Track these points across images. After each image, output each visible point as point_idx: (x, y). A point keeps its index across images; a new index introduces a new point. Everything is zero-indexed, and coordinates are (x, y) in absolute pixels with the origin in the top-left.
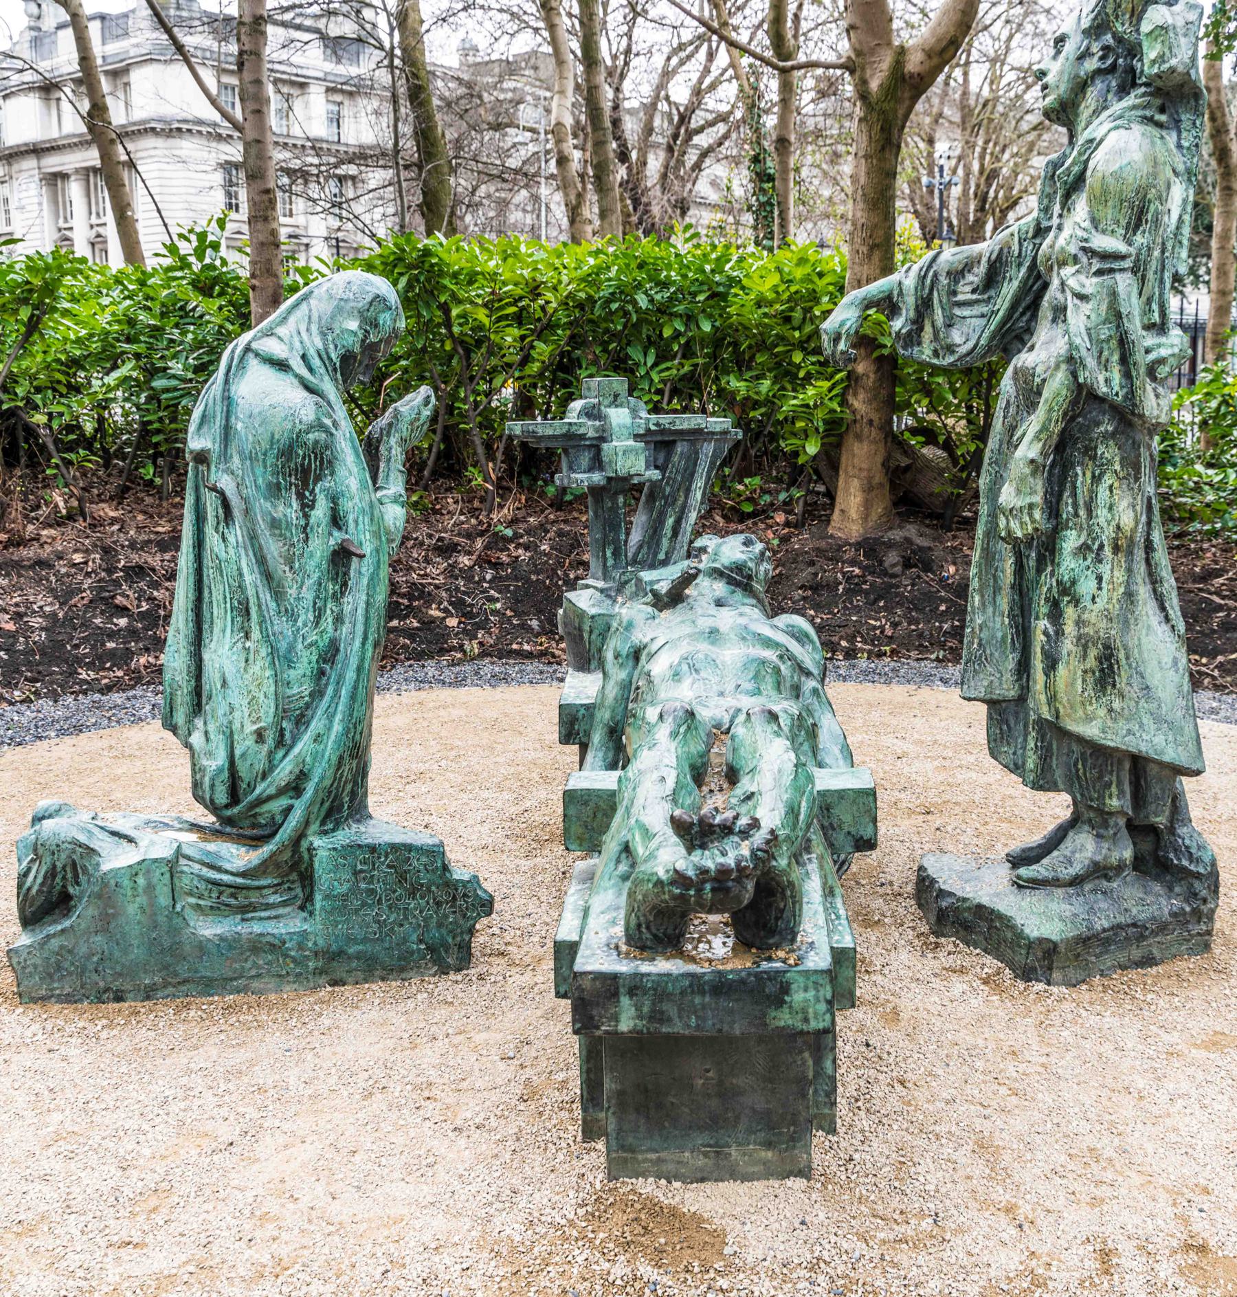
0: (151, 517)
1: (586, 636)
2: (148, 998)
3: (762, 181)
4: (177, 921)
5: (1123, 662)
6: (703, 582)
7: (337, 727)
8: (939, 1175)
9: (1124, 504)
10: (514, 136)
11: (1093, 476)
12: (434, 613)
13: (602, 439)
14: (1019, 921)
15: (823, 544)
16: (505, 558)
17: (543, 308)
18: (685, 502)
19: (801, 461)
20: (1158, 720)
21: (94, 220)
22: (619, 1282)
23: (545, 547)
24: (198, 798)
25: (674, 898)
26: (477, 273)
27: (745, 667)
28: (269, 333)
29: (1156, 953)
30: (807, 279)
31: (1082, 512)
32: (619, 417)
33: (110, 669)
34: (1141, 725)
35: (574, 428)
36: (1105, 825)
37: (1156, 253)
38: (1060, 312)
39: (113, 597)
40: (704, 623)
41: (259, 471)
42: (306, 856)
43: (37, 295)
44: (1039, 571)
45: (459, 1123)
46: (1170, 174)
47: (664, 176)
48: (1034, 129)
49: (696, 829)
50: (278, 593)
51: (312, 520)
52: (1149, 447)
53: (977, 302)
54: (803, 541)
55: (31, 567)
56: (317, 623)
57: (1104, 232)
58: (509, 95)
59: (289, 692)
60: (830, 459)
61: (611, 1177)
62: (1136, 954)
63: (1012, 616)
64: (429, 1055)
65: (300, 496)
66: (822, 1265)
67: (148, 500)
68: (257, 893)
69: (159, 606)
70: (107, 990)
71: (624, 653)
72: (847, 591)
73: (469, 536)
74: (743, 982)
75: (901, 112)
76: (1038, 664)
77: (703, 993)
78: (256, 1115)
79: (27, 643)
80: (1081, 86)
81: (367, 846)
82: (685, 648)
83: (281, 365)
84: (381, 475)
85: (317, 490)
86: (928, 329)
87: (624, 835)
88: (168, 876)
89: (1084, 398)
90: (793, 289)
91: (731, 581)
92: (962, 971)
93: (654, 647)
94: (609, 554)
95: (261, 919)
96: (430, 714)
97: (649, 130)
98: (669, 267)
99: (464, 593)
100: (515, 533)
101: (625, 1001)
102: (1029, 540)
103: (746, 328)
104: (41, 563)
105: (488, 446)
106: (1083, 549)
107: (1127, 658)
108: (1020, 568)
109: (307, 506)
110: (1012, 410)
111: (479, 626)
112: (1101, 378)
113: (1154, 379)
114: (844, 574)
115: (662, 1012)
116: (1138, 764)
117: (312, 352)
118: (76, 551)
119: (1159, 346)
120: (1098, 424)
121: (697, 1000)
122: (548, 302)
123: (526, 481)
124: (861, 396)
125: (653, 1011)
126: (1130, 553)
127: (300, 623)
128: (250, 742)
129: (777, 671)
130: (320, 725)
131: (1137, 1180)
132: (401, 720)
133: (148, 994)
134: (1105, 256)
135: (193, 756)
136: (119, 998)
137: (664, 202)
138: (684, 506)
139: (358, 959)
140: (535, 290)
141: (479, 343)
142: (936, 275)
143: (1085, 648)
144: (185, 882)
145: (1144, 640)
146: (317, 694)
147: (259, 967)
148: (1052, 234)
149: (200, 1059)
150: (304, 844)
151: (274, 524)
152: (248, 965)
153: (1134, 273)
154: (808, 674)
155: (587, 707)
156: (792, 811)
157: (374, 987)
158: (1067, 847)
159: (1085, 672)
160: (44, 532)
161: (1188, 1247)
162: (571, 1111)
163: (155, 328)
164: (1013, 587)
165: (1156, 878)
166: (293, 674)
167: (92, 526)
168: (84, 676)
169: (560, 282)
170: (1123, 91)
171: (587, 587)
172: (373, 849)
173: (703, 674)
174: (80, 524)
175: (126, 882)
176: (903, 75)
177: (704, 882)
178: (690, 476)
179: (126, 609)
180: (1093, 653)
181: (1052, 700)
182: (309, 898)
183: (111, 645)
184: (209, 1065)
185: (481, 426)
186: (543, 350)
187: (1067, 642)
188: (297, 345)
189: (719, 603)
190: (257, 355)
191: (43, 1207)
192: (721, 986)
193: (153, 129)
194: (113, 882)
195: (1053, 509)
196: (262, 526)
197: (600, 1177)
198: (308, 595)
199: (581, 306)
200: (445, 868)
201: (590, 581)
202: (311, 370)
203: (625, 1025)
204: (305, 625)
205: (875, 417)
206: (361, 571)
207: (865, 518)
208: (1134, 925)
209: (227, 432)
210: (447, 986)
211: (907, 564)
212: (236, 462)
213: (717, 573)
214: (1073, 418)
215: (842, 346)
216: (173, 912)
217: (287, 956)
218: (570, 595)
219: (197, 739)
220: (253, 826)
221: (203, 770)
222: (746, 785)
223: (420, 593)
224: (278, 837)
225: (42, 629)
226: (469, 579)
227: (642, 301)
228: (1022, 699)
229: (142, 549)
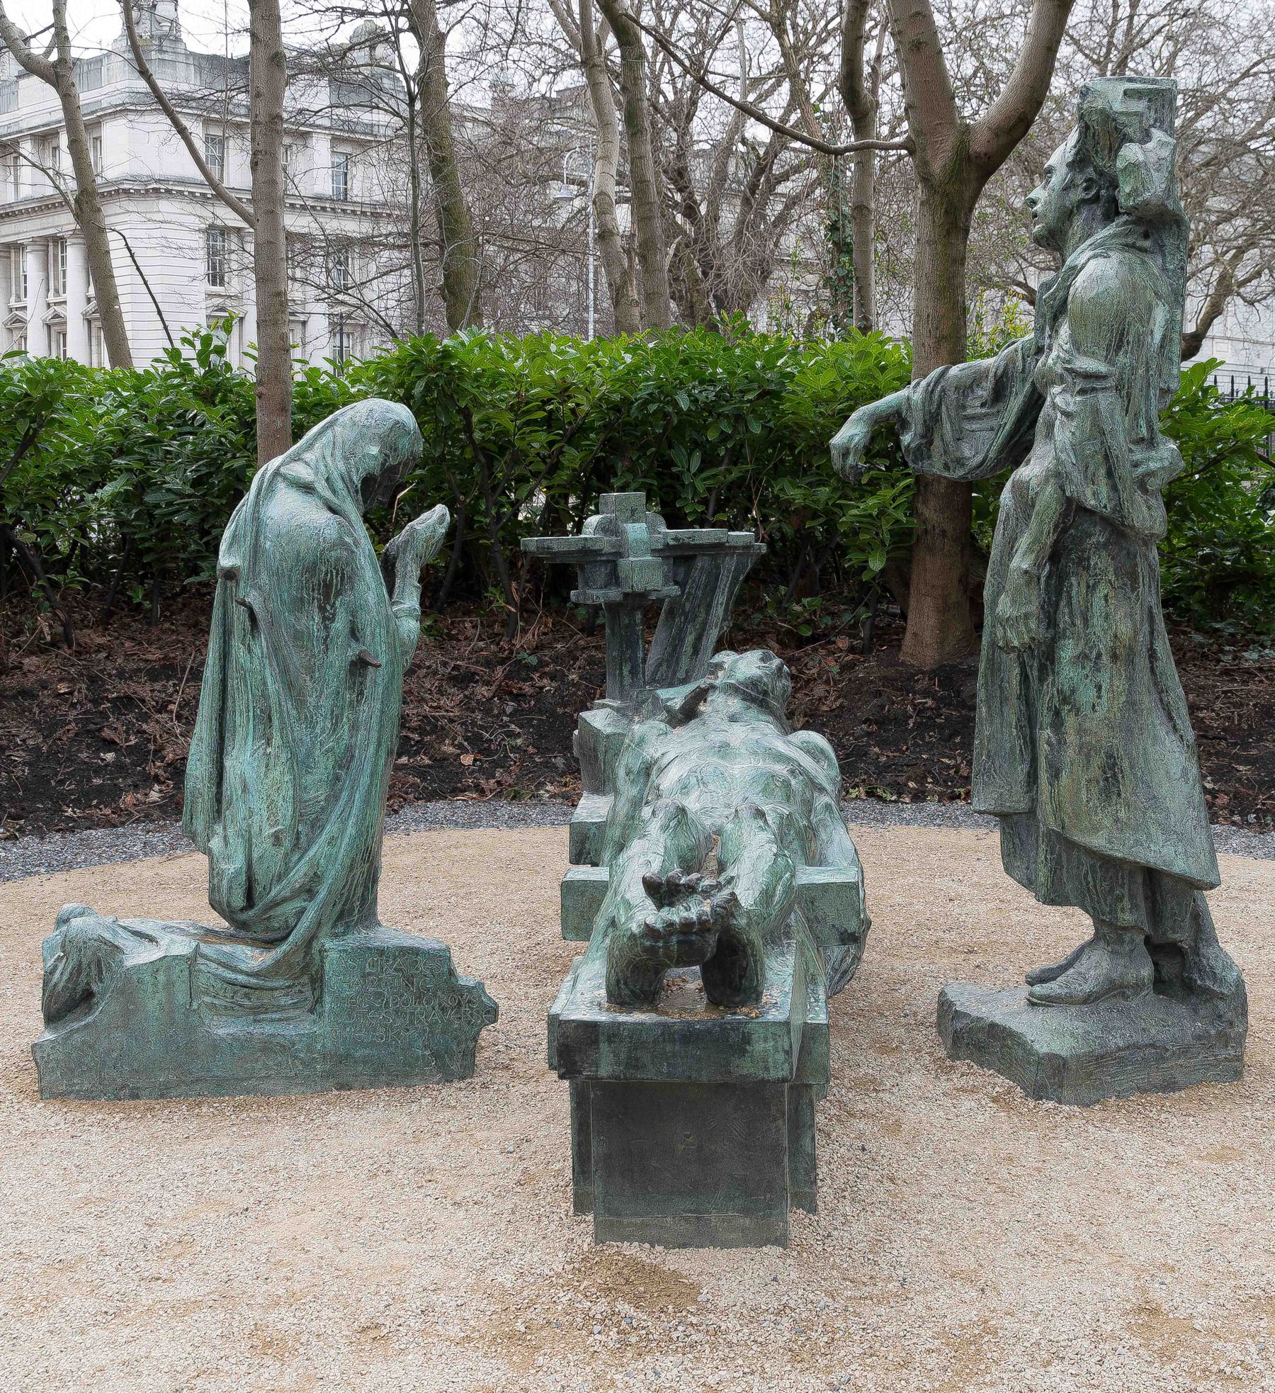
0: (140, 644)
1: (601, 757)
2: (162, 1096)
3: (840, 252)
4: (194, 1019)
5: (1127, 771)
6: (717, 699)
7: (351, 830)
8: (913, 1251)
9: (1121, 613)
10: (556, 190)
11: (1088, 587)
12: (448, 749)
13: (619, 555)
14: (1029, 1038)
15: (891, 672)
16: (527, 688)
17: (573, 411)
18: (706, 619)
19: (865, 577)
20: (1166, 830)
21: (52, 299)
22: (599, 1316)
23: (573, 677)
24: (214, 904)
25: (646, 950)
26: (502, 375)
27: (754, 780)
28: (296, 458)
29: (1180, 1078)
30: (868, 375)
31: (1078, 622)
32: (636, 531)
33: (96, 806)
34: (1149, 835)
35: (589, 544)
36: (1121, 941)
38: (1050, 426)
39: (100, 730)
40: (717, 738)
41: (285, 587)
42: (317, 958)
43: (34, 404)
44: (1042, 680)
45: (458, 1199)
46: (1150, 295)
47: (739, 233)
48: (1207, 164)
49: (664, 889)
50: (300, 703)
52: (1146, 558)
53: (986, 415)
54: (869, 669)
55: (14, 697)
56: (335, 726)
57: (1085, 354)
58: (553, 141)
59: (306, 797)
61: (598, 1240)
62: (1157, 1077)
63: (1020, 728)
64: (431, 1149)
65: (322, 609)
66: (788, 1311)
67: (135, 626)
68: (269, 993)
69: (149, 740)
71: (636, 769)
72: (918, 725)
73: (489, 664)
74: (709, 1032)
76: (1043, 776)
77: (673, 1041)
78: (268, 1189)
79: (10, 778)
80: (1068, 215)
81: (377, 949)
82: (694, 759)
83: (307, 488)
84: (396, 590)
85: (338, 604)
86: (937, 442)
87: (611, 911)
88: (187, 973)
90: (852, 386)
91: (747, 698)
92: (974, 1090)
93: (665, 761)
94: (625, 672)
95: (272, 1020)
96: (441, 853)
97: (721, 176)
98: (714, 364)
99: (482, 727)
100: (540, 661)
101: (604, 1047)
103: (803, 428)
104: (25, 693)
105: (512, 564)
107: (1132, 767)
108: (1025, 678)
109: (328, 619)
111: (496, 764)
112: (1089, 493)
114: (914, 706)
115: (637, 1059)
116: (1152, 877)
117: (336, 475)
118: (61, 680)
119: (1149, 459)
120: (1090, 535)
121: (669, 1048)
122: (578, 405)
123: (554, 602)
124: (932, 503)
125: (629, 1058)
126: (1131, 662)
128: (267, 845)
129: (787, 784)
130: (335, 829)
131: (1105, 1259)
132: (407, 860)
133: (163, 1093)
134: (1088, 376)
135: (211, 862)
136: (135, 1096)
137: (739, 264)
138: (704, 624)
139: (365, 1063)
140: (565, 392)
141: (502, 450)
142: (943, 390)
143: (1088, 756)
144: (202, 981)
147: (268, 1068)
149: (214, 1146)
150: (316, 946)
151: (297, 636)
153: (1118, 388)
154: (822, 790)
155: (599, 826)
156: (767, 896)
157: (380, 1092)
158: (1083, 965)
159: (1089, 781)
160: (26, 661)
161: (1141, 1310)
162: (565, 1192)
163: (151, 441)
165: (1183, 1001)
166: (309, 780)
167: (78, 654)
168: (69, 812)
169: (592, 383)
171: (604, 706)
172: (381, 952)
173: (711, 787)
174: (65, 651)
175: (147, 978)
176: (969, 158)
177: (671, 934)
178: (711, 590)
179: (114, 743)
180: (1097, 761)
181: (1058, 808)
182: (319, 1000)
183: (97, 781)
184: (222, 1150)
185: (503, 542)
186: (573, 458)
187: (1070, 752)
189: (733, 719)
190: (285, 478)
191: (79, 1252)
192: (689, 1036)
193: (126, 191)
194: (135, 977)
195: (1051, 620)
196: (286, 636)
197: (588, 1240)
198: (326, 703)
199: (616, 408)
200: (451, 973)
201: (606, 701)
202: (334, 492)
203: (604, 1071)
204: (323, 732)
205: (948, 527)
206: (377, 681)
207: (942, 642)
208: (1153, 1046)
209: (256, 552)
210: (450, 1093)
212: (264, 578)
213: (734, 689)
214: (1064, 531)
215: (851, 460)
216: (189, 1011)
217: (296, 1057)
218: (584, 714)
219: (216, 844)
220: (267, 929)
221: (220, 874)
222: (731, 872)
223: (431, 727)
224: (291, 939)
225: (24, 764)
226: (488, 712)
227: (684, 404)
228: (1032, 812)
229: (131, 678)
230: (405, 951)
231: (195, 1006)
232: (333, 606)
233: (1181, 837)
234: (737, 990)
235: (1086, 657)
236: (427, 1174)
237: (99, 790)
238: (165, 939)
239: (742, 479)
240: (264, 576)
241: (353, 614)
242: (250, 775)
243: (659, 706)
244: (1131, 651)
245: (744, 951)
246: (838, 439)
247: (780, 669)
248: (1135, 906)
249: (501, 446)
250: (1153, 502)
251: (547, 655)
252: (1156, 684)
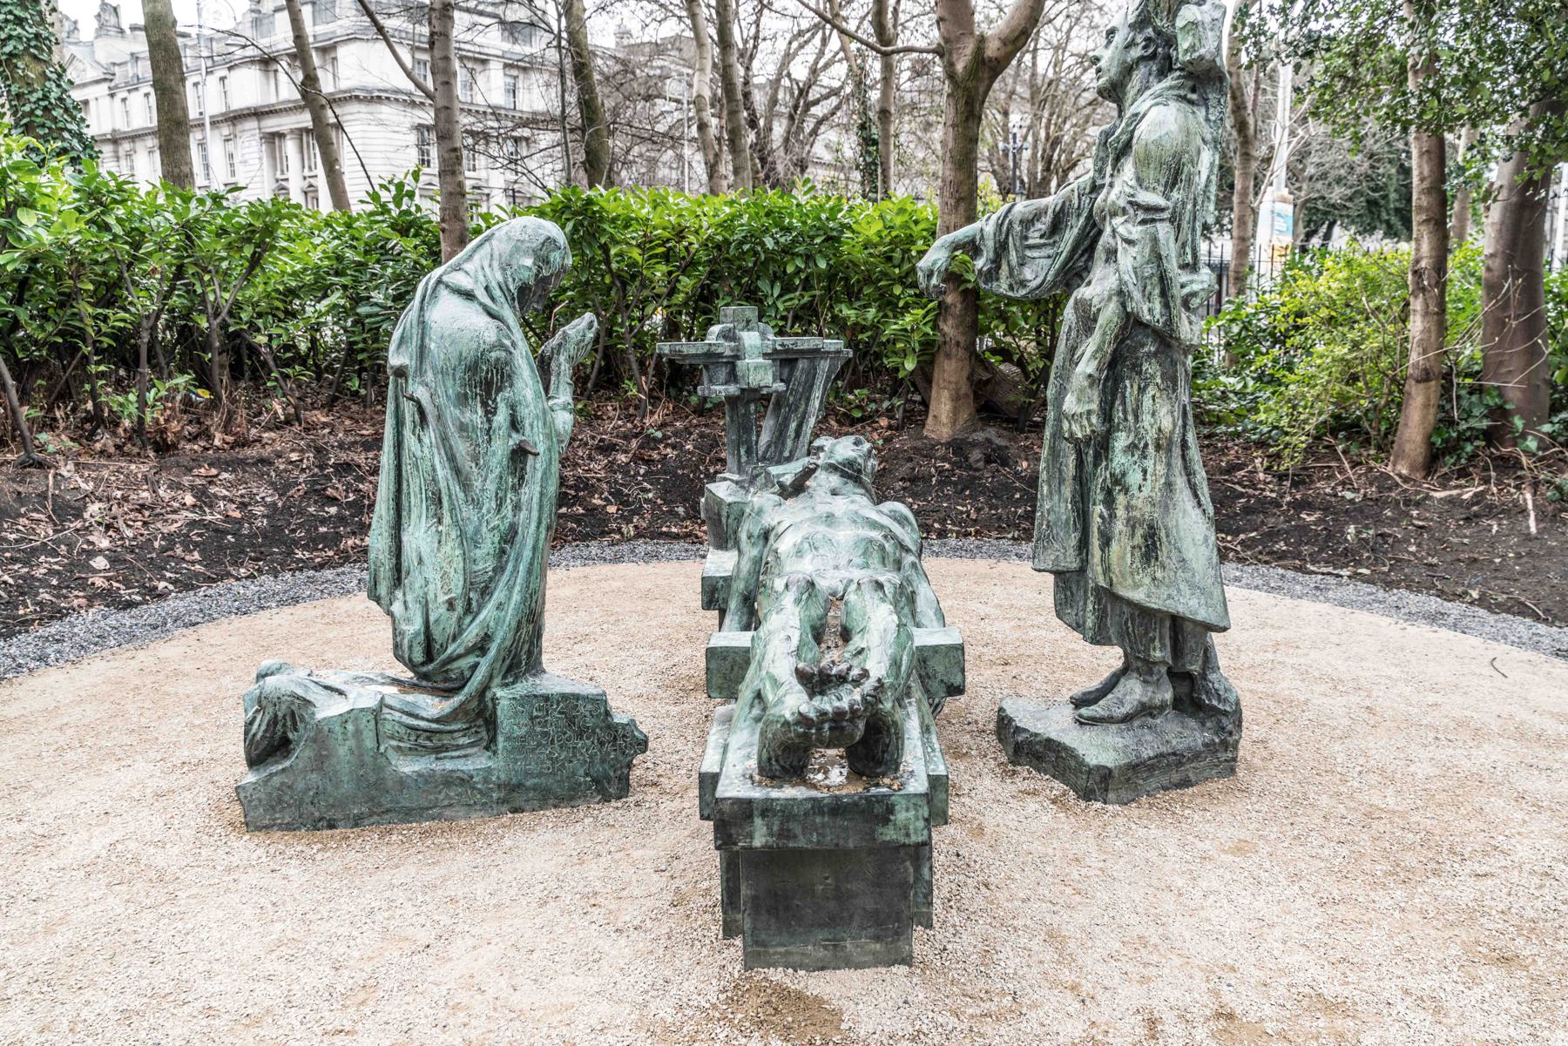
2: (356, 825)
4: (382, 760)
6: (821, 475)
7: (516, 597)
9: (1164, 411)
10: (661, 105)
12: (597, 501)
13: (737, 357)
14: (1081, 752)
15: (919, 444)
16: (655, 456)
17: (687, 248)
19: (901, 375)
20: (1193, 586)
21: (307, 173)
23: (689, 447)
24: (399, 657)
25: (799, 735)
28: (457, 268)
29: (1193, 778)
30: (905, 226)
31: (1130, 418)
32: (751, 339)
34: (1179, 590)
36: (1151, 673)
37: (1189, 207)
38: (1112, 254)
40: (822, 509)
41: (450, 383)
42: (490, 704)
45: (620, 925)
49: (816, 678)
50: (466, 486)
51: (494, 425)
53: (1044, 245)
54: (902, 442)
55: (255, 464)
56: (499, 506)
57: (1147, 189)
58: (658, 72)
59: (476, 568)
60: (925, 374)
61: (748, 967)
62: (1176, 777)
63: (1074, 503)
64: (594, 870)
65: (484, 404)
68: (449, 736)
70: (321, 819)
71: (756, 534)
73: (625, 437)
74: (856, 804)
75: (981, 90)
76: (1095, 542)
77: (823, 814)
78: (448, 922)
80: (1128, 70)
82: (805, 530)
83: (469, 296)
84: (552, 386)
86: (1004, 267)
87: (757, 684)
89: (1131, 323)
91: (844, 475)
92: (1035, 793)
93: (780, 529)
94: (742, 452)
97: (774, 101)
98: (791, 215)
101: (758, 822)
104: (263, 461)
106: (1132, 448)
108: (1080, 464)
109: (490, 413)
110: (1073, 334)
111: (634, 513)
112: (1145, 308)
113: (1188, 309)
116: (1176, 621)
117: (494, 284)
120: (1143, 346)
123: (673, 392)
124: (950, 322)
125: (781, 829)
128: (443, 610)
129: (882, 548)
130: (502, 595)
131: (1177, 961)
132: (568, 591)
133: (357, 822)
134: (1148, 209)
136: (331, 826)
138: (805, 412)
141: (633, 277)
142: (1011, 223)
144: (387, 728)
145: (1181, 522)
149: (400, 876)
150: (489, 695)
151: (462, 428)
152: (441, 796)
153: (1172, 220)
154: (908, 550)
155: (725, 579)
156: (896, 663)
161: (1219, 1015)
163: (360, 264)
164: (1074, 478)
168: (300, 555)
170: (1162, 74)
171: (725, 479)
172: (546, 698)
174: (296, 428)
175: (338, 729)
177: (823, 722)
180: (1139, 532)
181: (1107, 570)
182: (493, 740)
183: (323, 529)
184: (409, 880)
185: (635, 346)
186: (687, 283)
188: (481, 278)
189: (834, 493)
190: (447, 286)
192: (837, 808)
193: (357, 97)
195: (1107, 414)
198: (491, 487)
199: (718, 247)
200: (607, 713)
201: (727, 475)
202: (493, 299)
203: (758, 842)
205: (961, 339)
206: (535, 468)
207: (954, 423)
208: (1174, 754)
211: (988, 461)
212: (430, 376)
213: (833, 468)
214: (1122, 341)
215: (934, 281)
219: (397, 607)
220: (446, 680)
221: (402, 634)
222: (857, 642)
223: (585, 485)
224: (466, 690)
226: (626, 473)
227: (769, 243)
228: (1082, 570)
230: (565, 697)
231: (382, 749)
232: (494, 401)
233: (1203, 591)
234: (880, 763)
236: (591, 899)
237: (324, 537)
238: (353, 691)
239: (811, 302)
240: (430, 375)
241: (513, 407)
242: (425, 551)
243: (769, 481)
244: (1170, 441)
245: (888, 730)
247: (870, 452)
248: (1163, 646)
249: (634, 274)
251: (669, 431)
252: (1186, 468)
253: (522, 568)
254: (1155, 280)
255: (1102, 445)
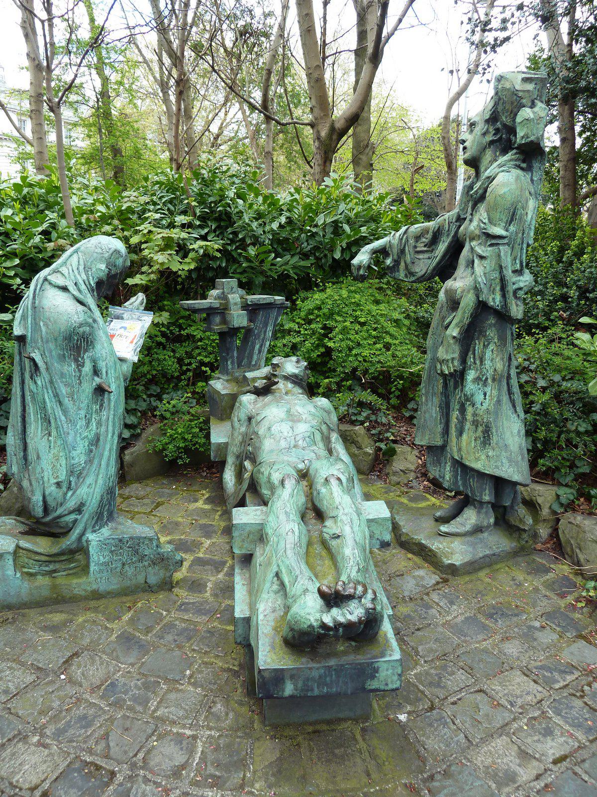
13: (226, 309)
28: (56, 271)
31: (478, 362)
37: (520, 235)
44: (455, 388)
53: (426, 251)
65: (76, 360)
75: (333, 146)
83: (65, 289)
86: (402, 264)
89: (482, 307)
91: (294, 382)
102: (451, 374)
106: (477, 380)
109: (80, 366)
112: (491, 300)
113: (516, 297)
126: (500, 381)
127: (78, 427)
128: (53, 488)
142: (407, 238)
146: (90, 461)
148: (467, 222)
150: (84, 539)
166: (74, 453)
170: (504, 152)
180: (480, 429)
181: (460, 450)
187: (468, 423)
188: (73, 277)
195: (464, 361)
202: (79, 291)
228: (443, 448)
235: (480, 379)
246: (355, 261)
250: (519, 303)
253: (104, 463)
254: (498, 280)
255: (459, 377)
